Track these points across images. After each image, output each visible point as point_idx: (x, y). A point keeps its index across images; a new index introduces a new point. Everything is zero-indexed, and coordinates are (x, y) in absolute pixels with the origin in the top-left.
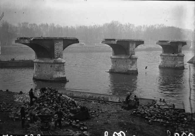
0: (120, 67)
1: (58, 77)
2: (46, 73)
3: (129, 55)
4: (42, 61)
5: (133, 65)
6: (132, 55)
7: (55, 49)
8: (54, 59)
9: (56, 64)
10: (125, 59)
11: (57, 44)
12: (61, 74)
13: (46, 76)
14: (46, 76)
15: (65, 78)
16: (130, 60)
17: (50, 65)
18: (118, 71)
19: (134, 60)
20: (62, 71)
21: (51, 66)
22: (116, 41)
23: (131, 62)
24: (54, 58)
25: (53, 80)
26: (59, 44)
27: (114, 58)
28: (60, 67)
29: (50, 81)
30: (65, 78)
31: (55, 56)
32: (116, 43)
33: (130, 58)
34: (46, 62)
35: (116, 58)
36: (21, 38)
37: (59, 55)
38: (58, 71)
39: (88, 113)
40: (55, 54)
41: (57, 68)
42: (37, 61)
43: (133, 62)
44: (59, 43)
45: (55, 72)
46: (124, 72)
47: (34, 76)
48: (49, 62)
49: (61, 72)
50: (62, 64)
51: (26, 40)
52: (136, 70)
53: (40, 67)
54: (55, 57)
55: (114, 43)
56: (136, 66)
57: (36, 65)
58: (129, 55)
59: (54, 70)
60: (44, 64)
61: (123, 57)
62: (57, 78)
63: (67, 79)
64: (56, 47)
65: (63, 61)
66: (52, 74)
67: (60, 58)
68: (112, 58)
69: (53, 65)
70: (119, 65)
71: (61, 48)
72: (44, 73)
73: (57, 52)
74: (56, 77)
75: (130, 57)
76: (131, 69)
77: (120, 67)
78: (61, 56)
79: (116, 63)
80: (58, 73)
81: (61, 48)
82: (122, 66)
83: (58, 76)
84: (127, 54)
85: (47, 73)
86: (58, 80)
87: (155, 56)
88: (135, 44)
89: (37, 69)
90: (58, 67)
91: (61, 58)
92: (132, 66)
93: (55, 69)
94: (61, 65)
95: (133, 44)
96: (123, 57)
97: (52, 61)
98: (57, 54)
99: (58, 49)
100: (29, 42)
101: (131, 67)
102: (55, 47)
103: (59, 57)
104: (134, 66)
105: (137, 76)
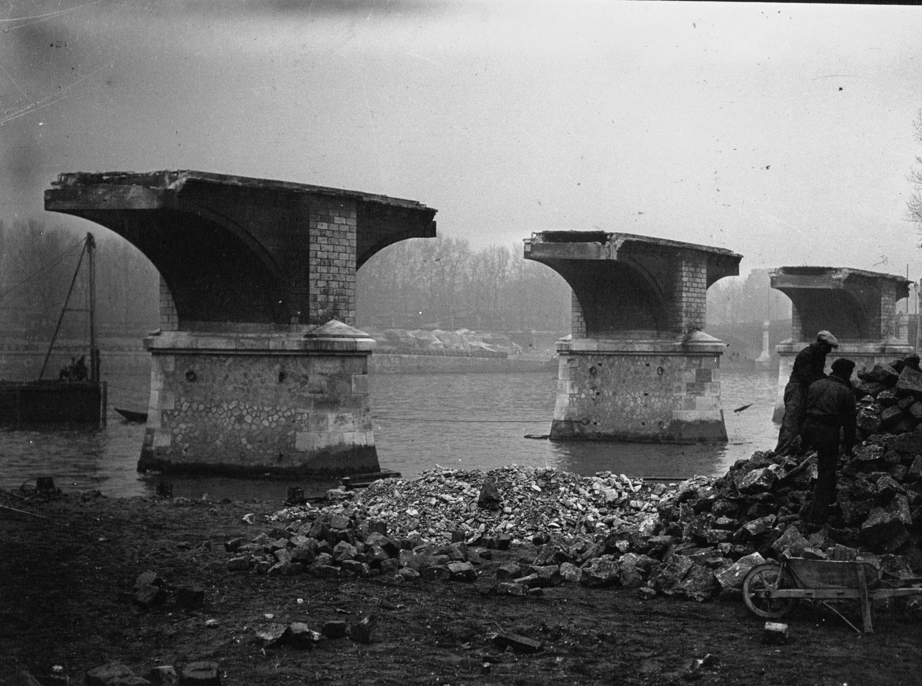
0: (624, 405)
1: (329, 448)
2: (240, 419)
3: (679, 331)
4: (220, 344)
5: (703, 389)
6: (690, 332)
7: (313, 262)
8: (306, 329)
9: (319, 357)
10: (654, 355)
11: (325, 226)
12: (350, 425)
13: (244, 441)
14: (244, 441)
15: (370, 451)
16: (683, 362)
17: (277, 367)
18: (610, 431)
19: (705, 363)
20: (356, 403)
21: (282, 376)
22: (619, 243)
23: (690, 376)
24: (305, 319)
25: (298, 464)
26: (333, 227)
27: (583, 354)
28: (344, 376)
29: (277, 471)
30: (370, 451)
31: (312, 306)
32: (614, 256)
33: (690, 351)
34: (248, 344)
35: (597, 354)
36: (89, 181)
37: (331, 298)
38: (332, 403)
39: (890, 522)
40: (313, 291)
41: (324, 383)
42: (181, 345)
43: (699, 373)
44: (337, 220)
45: (310, 412)
46: (651, 430)
47: (146, 445)
48: (272, 345)
49: (348, 415)
50: (357, 362)
51: (135, 191)
52: (719, 419)
53: (195, 384)
54: (313, 314)
55: (603, 257)
56: (718, 397)
57: (171, 368)
58: (679, 331)
59: (307, 403)
60: (231, 360)
61: (643, 346)
62: (324, 453)
63: (385, 461)
64: (319, 248)
65: (366, 341)
66: (287, 427)
67: (339, 324)
68: (572, 353)
69: (292, 367)
70: (614, 394)
71: (344, 256)
72: (228, 423)
73: (321, 284)
74: (322, 443)
75: (683, 345)
76: (691, 416)
77: (624, 405)
78: (342, 306)
79: (598, 380)
80: (331, 416)
81: (344, 256)
82: (635, 399)
83: (335, 441)
84: (666, 329)
85: (248, 419)
86: (333, 466)
87: (443, 478)
88: (704, 271)
89: (171, 397)
90: (332, 379)
91: (343, 320)
92: (698, 394)
93: (307, 395)
94: (348, 362)
95: (696, 267)
96: (643, 346)
97: (293, 340)
98: (326, 292)
99: (328, 263)
100: (155, 204)
101: (691, 405)
102: (313, 247)
103: (335, 314)
104: (707, 397)
105: (720, 461)
